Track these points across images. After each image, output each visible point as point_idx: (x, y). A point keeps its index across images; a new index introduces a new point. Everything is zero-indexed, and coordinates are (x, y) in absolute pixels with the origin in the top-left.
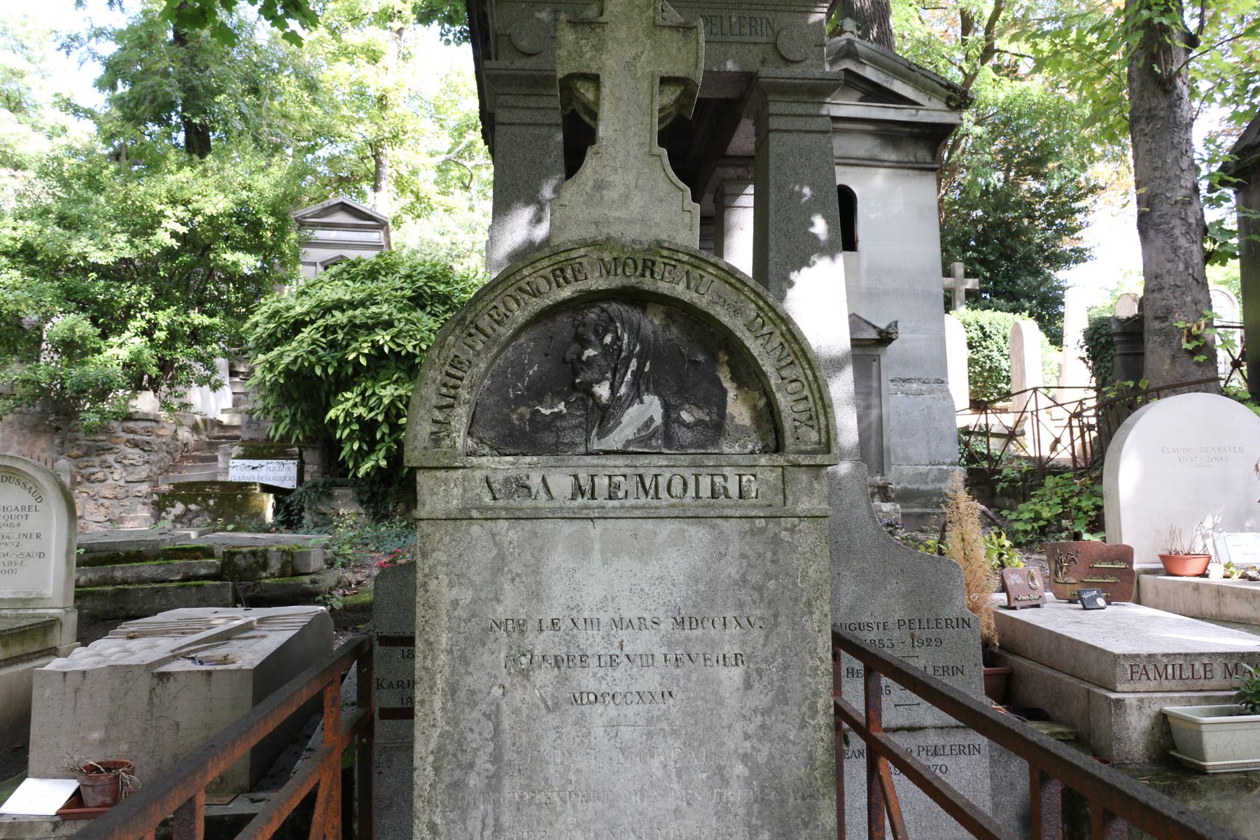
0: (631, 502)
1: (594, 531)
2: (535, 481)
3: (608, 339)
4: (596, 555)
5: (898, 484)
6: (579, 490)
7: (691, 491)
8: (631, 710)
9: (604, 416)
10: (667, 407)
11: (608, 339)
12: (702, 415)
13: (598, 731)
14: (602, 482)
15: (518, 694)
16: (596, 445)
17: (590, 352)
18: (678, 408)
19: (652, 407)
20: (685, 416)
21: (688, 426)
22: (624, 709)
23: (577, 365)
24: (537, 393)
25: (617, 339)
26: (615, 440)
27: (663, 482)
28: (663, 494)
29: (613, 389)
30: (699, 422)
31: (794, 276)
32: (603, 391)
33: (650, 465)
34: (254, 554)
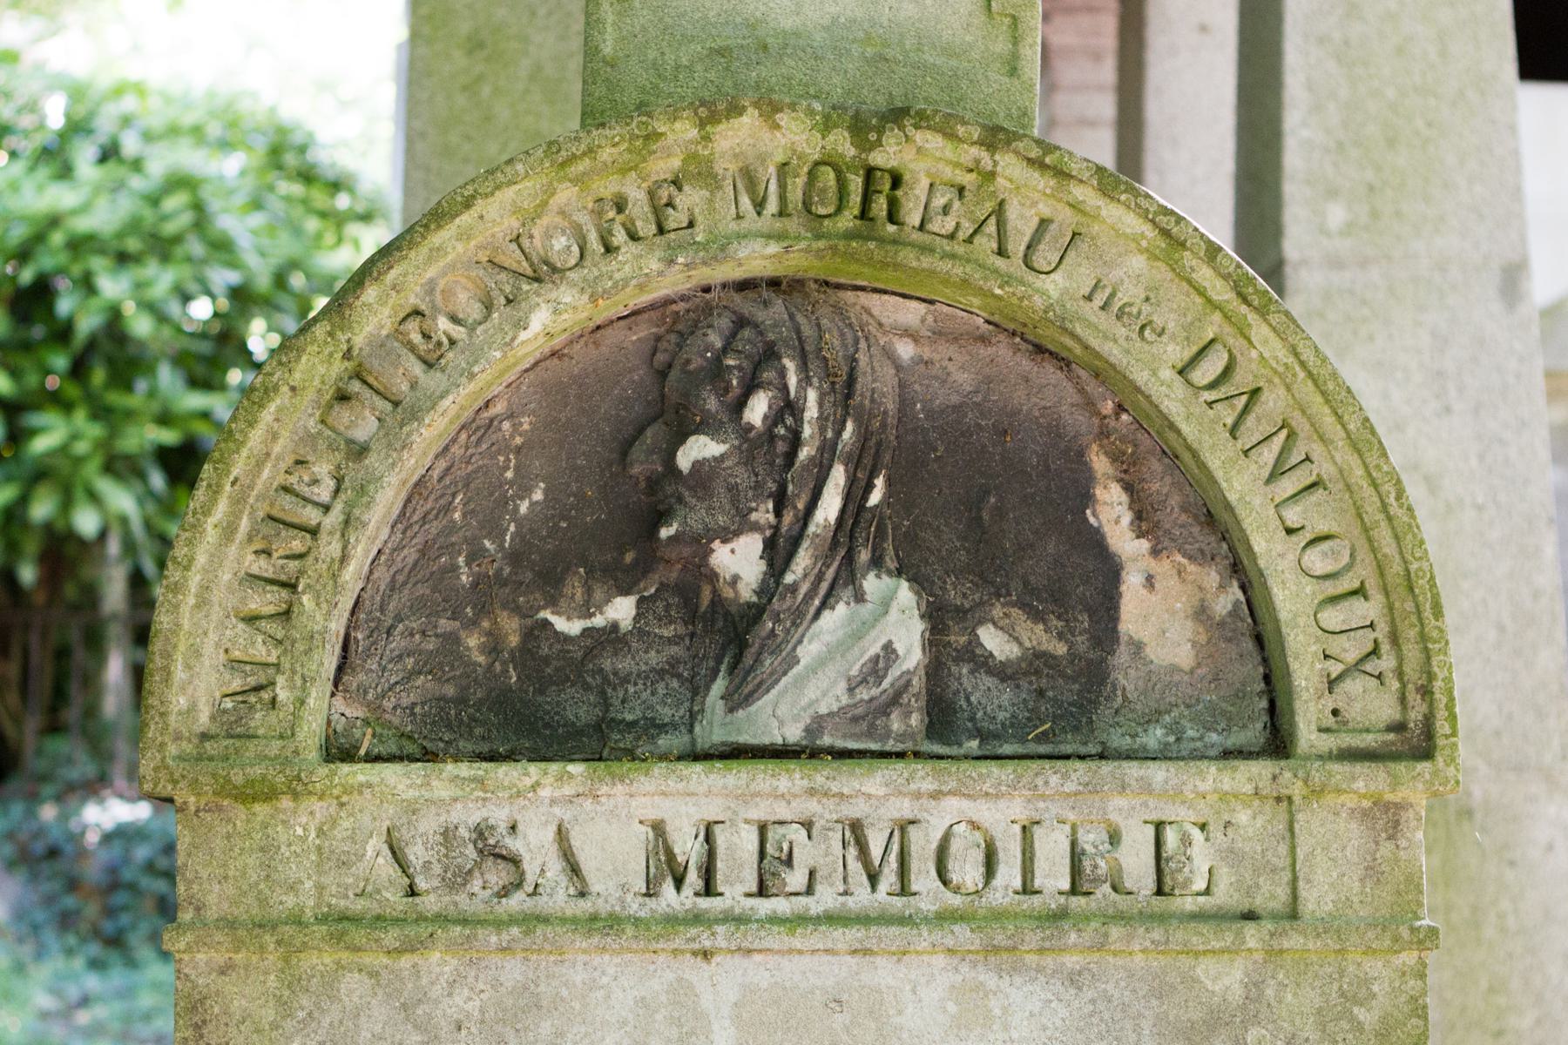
0: (826, 898)
2: (535, 846)
3: (757, 410)
7: (1009, 874)
9: (735, 640)
10: (939, 618)
11: (757, 410)
12: (1038, 636)
14: (739, 845)
16: (716, 727)
17: (698, 449)
18: (970, 616)
20: (993, 641)
21: (1004, 673)
24: (544, 568)
25: (788, 408)
26: (779, 715)
27: (923, 845)
28: (924, 879)
29: (778, 553)
30: (1037, 661)
32: (739, 561)
33: (877, 793)
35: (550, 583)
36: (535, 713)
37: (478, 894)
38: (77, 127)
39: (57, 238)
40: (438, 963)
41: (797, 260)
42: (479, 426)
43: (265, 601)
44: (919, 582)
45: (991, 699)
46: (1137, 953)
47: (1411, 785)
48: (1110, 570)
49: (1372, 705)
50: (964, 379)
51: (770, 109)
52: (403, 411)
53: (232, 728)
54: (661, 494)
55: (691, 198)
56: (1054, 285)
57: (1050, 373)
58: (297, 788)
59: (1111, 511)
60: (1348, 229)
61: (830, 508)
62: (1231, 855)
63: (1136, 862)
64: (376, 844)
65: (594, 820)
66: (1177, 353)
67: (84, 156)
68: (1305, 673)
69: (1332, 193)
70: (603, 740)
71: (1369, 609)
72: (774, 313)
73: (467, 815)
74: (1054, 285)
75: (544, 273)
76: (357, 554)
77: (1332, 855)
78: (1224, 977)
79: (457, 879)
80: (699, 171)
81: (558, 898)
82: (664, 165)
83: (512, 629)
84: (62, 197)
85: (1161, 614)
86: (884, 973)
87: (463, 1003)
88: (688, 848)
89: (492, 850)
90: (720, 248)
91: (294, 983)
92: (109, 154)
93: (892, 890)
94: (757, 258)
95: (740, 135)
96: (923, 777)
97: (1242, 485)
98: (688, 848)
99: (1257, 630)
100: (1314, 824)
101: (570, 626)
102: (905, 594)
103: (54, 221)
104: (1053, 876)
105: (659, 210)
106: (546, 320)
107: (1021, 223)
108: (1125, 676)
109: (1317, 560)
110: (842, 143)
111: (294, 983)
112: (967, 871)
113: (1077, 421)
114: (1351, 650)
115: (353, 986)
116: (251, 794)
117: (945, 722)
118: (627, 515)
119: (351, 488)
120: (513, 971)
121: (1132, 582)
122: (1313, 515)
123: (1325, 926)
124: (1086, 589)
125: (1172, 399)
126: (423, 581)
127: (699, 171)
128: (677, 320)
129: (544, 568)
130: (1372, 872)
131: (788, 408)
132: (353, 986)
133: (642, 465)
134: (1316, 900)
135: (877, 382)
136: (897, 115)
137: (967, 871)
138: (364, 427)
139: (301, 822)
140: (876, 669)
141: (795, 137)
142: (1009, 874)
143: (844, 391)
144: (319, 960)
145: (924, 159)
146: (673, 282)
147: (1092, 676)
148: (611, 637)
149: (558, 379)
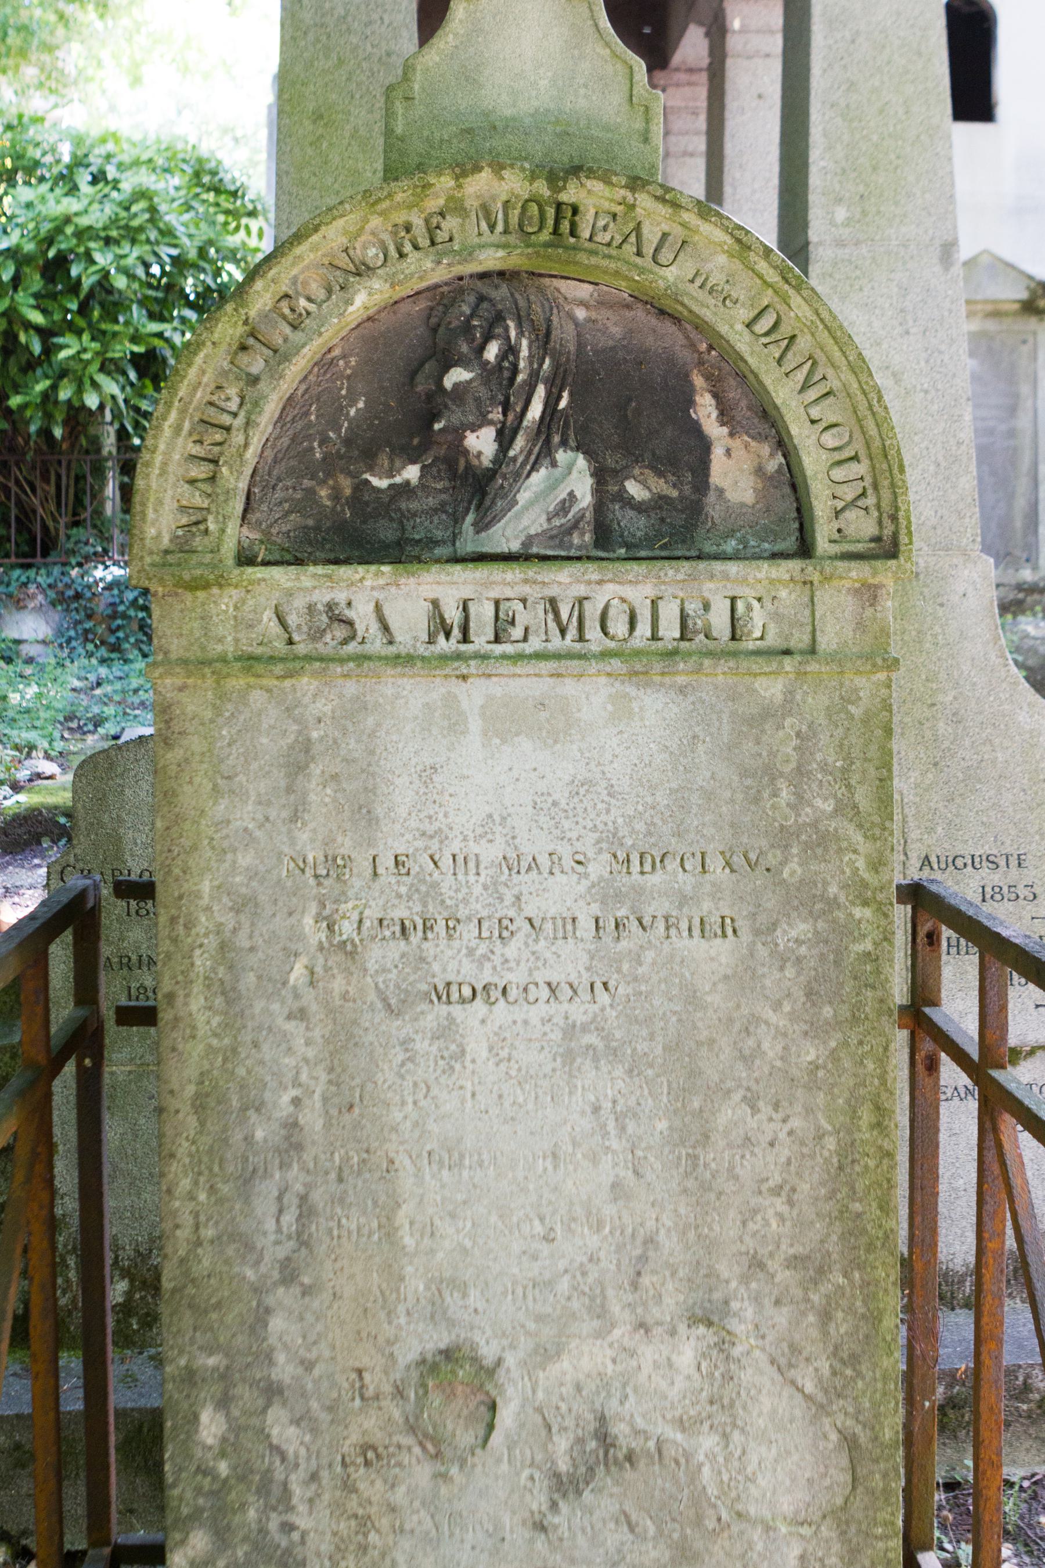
0: (535, 644)
1: (475, 694)
2: (362, 614)
3: (492, 352)
7: (644, 629)
8: (535, 1014)
9: (480, 490)
11: (492, 352)
12: (661, 486)
13: (477, 1047)
14: (483, 613)
15: (338, 985)
16: (469, 542)
17: (457, 375)
18: (620, 474)
19: (574, 477)
20: (634, 489)
21: (640, 508)
22: (519, 1013)
24: (366, 448)
26: (506, 535)
27: (592, 612)
28: (593, 632)
29: (505, 438)
30: (660, 502)
32: (482, 443)
33: (565, 582)
35: (369, 457)
38: (79, 162)
39: (69, 230)
40: (307, 684)
41: (516, 260)
42: (325, 363)
43: (200, 471)
45: (635, 525)
48: (705, 446)
49: (862, 526)
51: (498, 168)
52: (280, 356)
55: (451, 223)
56: (671, 274)
57: (668, 327)
58: (222, 582)
59: (705, 410)
60: (848, 222)
61: (536, 410)
63: (719, 621)
64: (268, 616)
66: (745, 314)
67: (83, 178)
68: (821, 507)
69: (839, 200)
72: (501, 292)
75: (362, 270)
76: (254, 442)
78: (771, 688)
80: (455, 206)
81: (377, 645)
82: (434, 204)
84: (71, 205)
85: (734, 472)
86: (569, 688)
87: (323, 707)
88: (453, 615)
89: (337, 617)
90: (468, 253)
91: (223, 696)
93: (574, 641)
94: (491, 259)
95: (480, 185)
96: (592, 571)
97: (784, 394)
98: (453, 615)
99: (792, 480)
101: (380, 483)
102: (581, 462)
103: (67, 220)
104: (670, 629)
105: (432, 231)
106: (363, 300)
107: (651, 235)
108: (713, 509)
109: (830, 440)
110: (542, 188)
111: (223, 696)
112: (619, 627)
113: (685, 355)
114: (849, 493)
115: (257, 697)
117: (605, 538)
118: (416, 419)
119: (249, 403)
120: (351, 688)
121: (717, 453)
123: (836, 658)
125: (742, 342)
126: (294, 457)
127: (455, 206)
128: (442, 298)
129: (366, 448)
130: (860, 626)
132: (257, 697)
134: (827, 642)
135: (564, 334)
136: (575, 170)
137: (619, 627)
138: (256, 365)
139: (224, 602)
140: (563, 508)
141: (513, 184)
142: (644, 629)
143: (544, 340)
144: (237, 683)
145: (591, 197)
146: (440, 274)
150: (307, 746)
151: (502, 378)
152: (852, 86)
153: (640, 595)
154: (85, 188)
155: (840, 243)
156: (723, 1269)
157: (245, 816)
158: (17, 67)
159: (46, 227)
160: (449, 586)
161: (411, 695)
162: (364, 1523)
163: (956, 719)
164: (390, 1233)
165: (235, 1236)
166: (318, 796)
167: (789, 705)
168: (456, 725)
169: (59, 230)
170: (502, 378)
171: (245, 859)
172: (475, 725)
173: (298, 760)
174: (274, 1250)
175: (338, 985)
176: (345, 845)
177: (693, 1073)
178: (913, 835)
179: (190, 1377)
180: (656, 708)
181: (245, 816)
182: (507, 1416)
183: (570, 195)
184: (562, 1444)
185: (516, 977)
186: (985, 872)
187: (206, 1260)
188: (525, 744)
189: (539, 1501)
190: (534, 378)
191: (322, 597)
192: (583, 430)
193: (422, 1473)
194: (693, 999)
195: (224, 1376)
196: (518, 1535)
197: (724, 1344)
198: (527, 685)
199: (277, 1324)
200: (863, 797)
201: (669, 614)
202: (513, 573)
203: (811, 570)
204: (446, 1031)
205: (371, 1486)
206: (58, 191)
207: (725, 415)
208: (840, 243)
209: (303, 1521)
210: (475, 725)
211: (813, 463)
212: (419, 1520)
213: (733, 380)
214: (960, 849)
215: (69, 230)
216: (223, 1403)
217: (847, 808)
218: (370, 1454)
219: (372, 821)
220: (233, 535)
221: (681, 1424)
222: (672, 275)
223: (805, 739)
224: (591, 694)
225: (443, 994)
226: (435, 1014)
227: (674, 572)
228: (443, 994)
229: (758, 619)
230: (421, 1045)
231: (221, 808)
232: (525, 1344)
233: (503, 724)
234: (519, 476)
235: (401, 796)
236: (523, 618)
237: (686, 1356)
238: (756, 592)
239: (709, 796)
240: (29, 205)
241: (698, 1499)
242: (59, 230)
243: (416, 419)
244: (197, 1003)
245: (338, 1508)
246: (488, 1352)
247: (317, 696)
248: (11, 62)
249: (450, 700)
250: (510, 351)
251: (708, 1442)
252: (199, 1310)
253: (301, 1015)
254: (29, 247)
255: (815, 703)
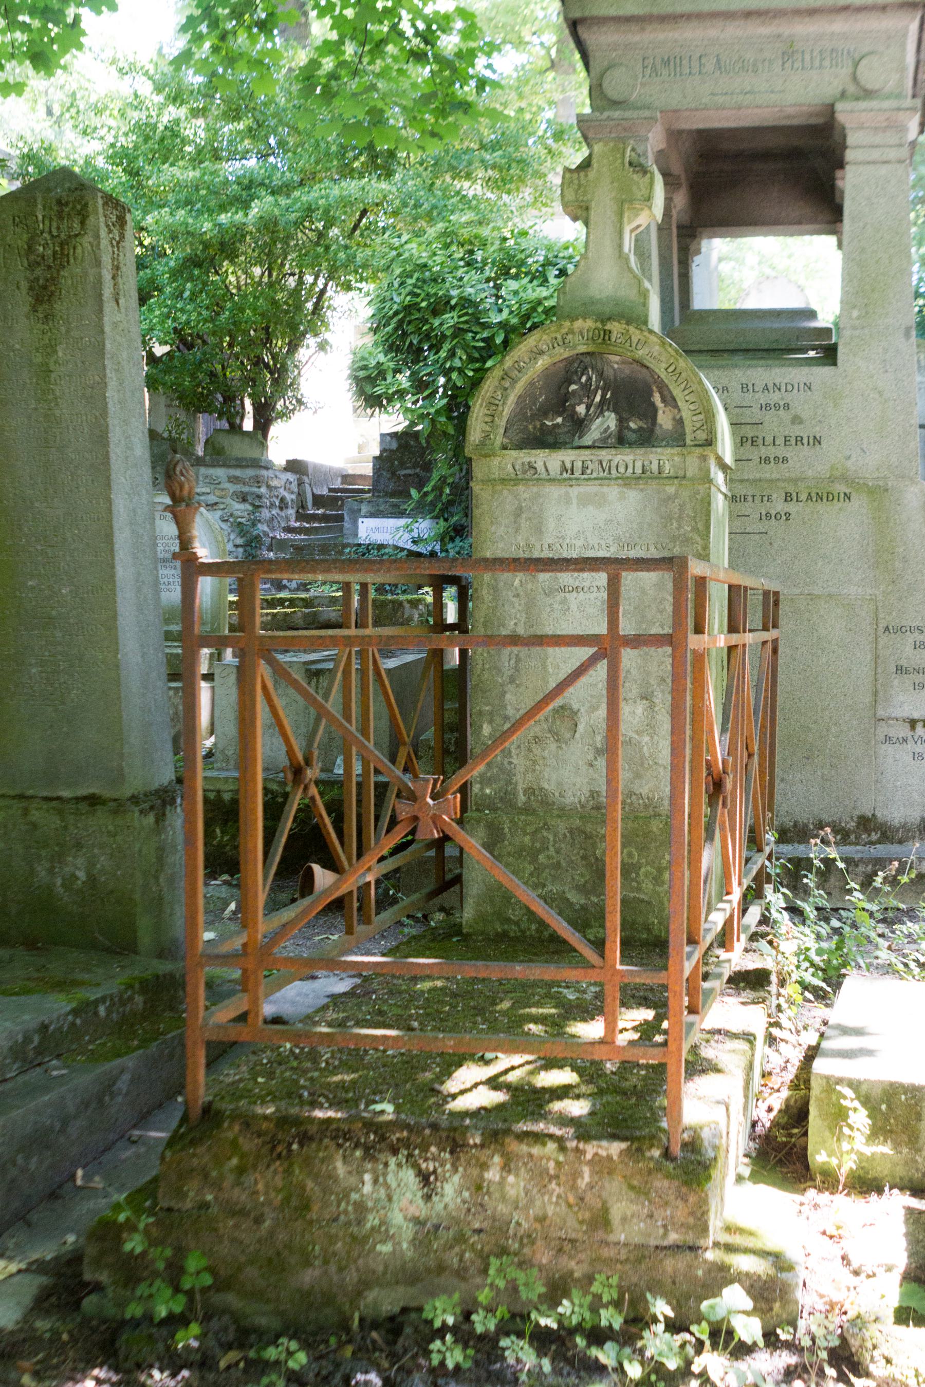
0: (595, 475)
1: (574, 492)
2: (539, 466)
3: (584, 379)
4: (574, 505)
5: (115, 325)
6: (564, 469)
7: (630, 470)
8: (592, 596)
9: (579, 425)
10: (621, 421)
11: (584, 379)
12: (641, 424)
13: (574, 607)
14: (578, 465)
15: (529, 586)
16: (577, 442)
17: (573, 387)
18: (628, 420)
19: (610, 421)
20: (632, 425)
21: (634, 431)
22: (587, 596)
23: (566, 397)
24: (545, 412)
25: (589, 379)
26: (587, 440)
27: (614, 464)
28: (614, 471)
29: (588, 408)
30: (640, 429)
31: (367, 469)
32: (581, 409)
33: (604, 455)
34: (119, 698)
35: (545, 415)
36: (544, 440)
37: (529, 475)
38: (547, 263)
39: (540, 309)
40: (521, 488)
41: (590, 349)
42: (532, 384)
43: (488, 419)
44: (617, 413)
45: (632, 437)
46: (654, 485)
47: (707, 451)
48: (655, 410)
49: (702, 436)
50: (627, 372)
51: (584, 319)
52: (514, 381)
53: (482, 443)
54: (566, 397)
55: (570, 337)
56: (640, 352)
57: (644, 370)
58: (494, 455)
59: (657, 398)
60: (858, 318)
61: (598, 399)
62: (673, 466)
63: (655, 467)
64: (509, 466)
65: (550, 461)
66: (664, 365)
67: (552, 272)
68: (688, 429)
69: (854, 307)
70: (555, 446)
71: (701, 417)
72: (587, 360)
73: (526, 460)
74: (640, 352)
75: (541, 353)
76: (508, 409)
77: (692, 466)
78: (671, 490)
79: (525, 472)
80: (571, 331)
81: (544, 475)
82: (564, 331)
83: (538, 424)
84: (543, 292)
85: (665, 419)
86: (605, 489)
87: (526, 495)
88: (568, 466)
89: (532, 467)
90: (574, 347)
91: (494, 492)
92: (563, 273)
93: (607, 475)
94: (582, 349)
95: (579, 324)
96: (613, 451)
97: (677, 392)
98: (568, 466)
99: (680, 422)
100: (689, 459)
101: (549, 423)
102: (613, 415)
103: (539, 302)
104: (639, 471)
105: (564, 339)
106: (541, 363)
107: (635, 340)
108: (658, 431)
109: (692, 407)
110: (599, 325)
111: (494, 492)
112: (622, 470)
113: (650, 380)
114: (698, 425)
115: (505, 492)
116: (486, 456)
117: (621, 440)
118: (560, 402)
119: (505, 397)
120: (535, 489)
121: (660, 412)
122: (691, 398)
123: (692, 480)
124: (651, 414)
125: (663, 375)
126: (520, 415)
127: (571, 331)
128: (569, 361)
129: (545, 412)
130: (700, 469)
131: (589, 379)
132: (505, 492)
133: (563, 391)
134: (689, 474)
135: (609, 373)
136: (609, 319)
137: (622, 470)
138: (507, 384)
139: (496, 461)
140: (606, 430)
141: (590, 323)
142: (630, 470)
143: (601, 375)
144: (499, 488)
145: (615, 327)
146: (566, 354)
147: (652, 431)
148: (557, 425)
149: (547, 374)
150: (520, 509)
151: (586, 387)
152: (863, 250)
153: (629, 458)
154: (553, 281)
155: (854, 328)
156: (652, 681)
157: (501, 531)
158: (518, 189)
159: (526, 307)
160: (567, 456)
161: (554, 492)
162: (535, 762)
163: (905, 560)
164: (544, 667)
165: (496, 668)
166: (524, 524)
167: (676, 496)
168: (568, 501)
169: (534, 309)
170: (586, 387)
171: (501, 545)
172: (575, 501)
173: (518, 512)
174: (508, 673)
175: (529, 586)
176: (533, 540)
177: (643, 617)
178: (881, 616)
179: (480, 713)
180: (633, 496)
181: (501, 531)
182: (581, 728)
183: (608, 327)
184: (599, 738)
185: (586, 584)
186: (916, 634)
187: (486, 675)
188: (591, 508)
189: (591, 756)
190: (597, 388)
191: (526, 460)
192: (615, 405)
193: (553, 746)
194: (643, 592)
195: (491, 713)
196: (584, 768)
197: (652, 707)
198: (591, 489)
199: (508, 696)
200: (700, 526)
201: (639, 465)
202: (587, 452)
203: (685, 451)
204: (564, 601)
205: (536, 750)
206: (535, 282)
207: (664, 400)
208: (854, 328)
209: (515, 761)
210: (575, 501)
211: (686, 414)
212: (552, 762)
213: (663, 388)
214: (904, 623)
215: (540, 309)
216: (490, 722)
217: (695, 529)
218: (537, 740)
219: (541, 532)
220: (499, 440)
221: (637, 732)
222: (641, 353)
223: (682, 507)
224: (612, 492)
225: (563, 589)
226: (560, 596)
227: (640, 451)
228: (563, 589)
229: (667, 468)
230: (556, 606)
231: (493, 529)
232: (587, 705)
233: (584, 501)
234: (592, 421)
235: (551, 525)
236: (591, 466)
237: (639, 710)
238: (662, 458)
239: (650, 525)
240: (516, 293)
241: (642, 757)
242: (534, 309)
243: (560, 402)
244: (485, 592)
245: (526, 758)
246: (575, 707)
247: (524, 492)
248: (513, 186)
249: (567, 494)
250: (589, 379)
251: (646, 739)
252: (484, 692)
253: (517, 596)
254: (514, 321)
255: (685, 494)
